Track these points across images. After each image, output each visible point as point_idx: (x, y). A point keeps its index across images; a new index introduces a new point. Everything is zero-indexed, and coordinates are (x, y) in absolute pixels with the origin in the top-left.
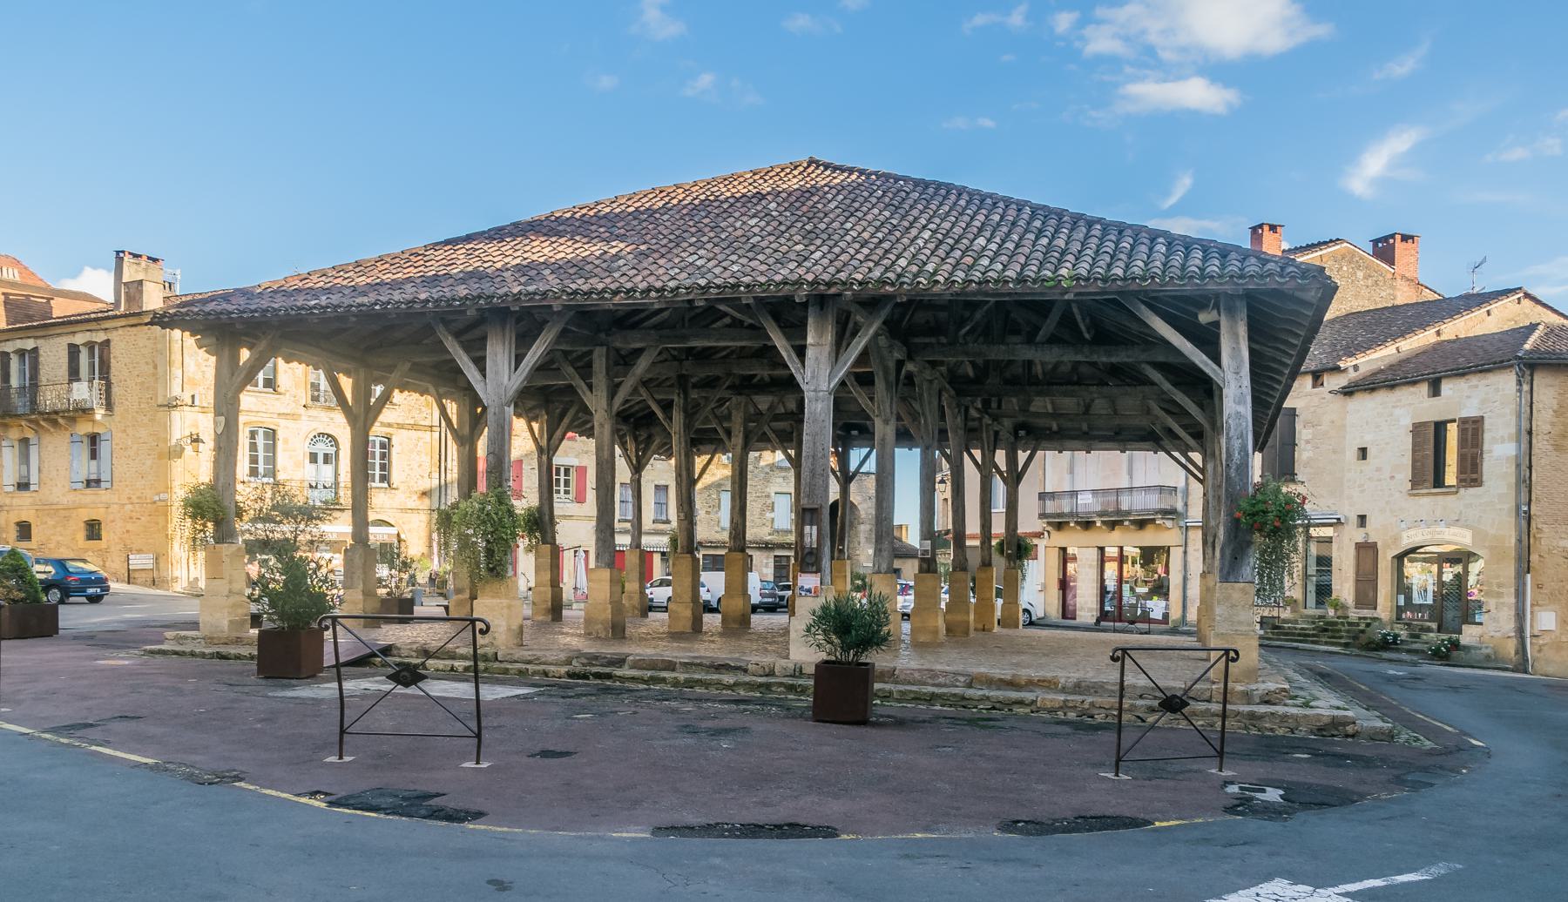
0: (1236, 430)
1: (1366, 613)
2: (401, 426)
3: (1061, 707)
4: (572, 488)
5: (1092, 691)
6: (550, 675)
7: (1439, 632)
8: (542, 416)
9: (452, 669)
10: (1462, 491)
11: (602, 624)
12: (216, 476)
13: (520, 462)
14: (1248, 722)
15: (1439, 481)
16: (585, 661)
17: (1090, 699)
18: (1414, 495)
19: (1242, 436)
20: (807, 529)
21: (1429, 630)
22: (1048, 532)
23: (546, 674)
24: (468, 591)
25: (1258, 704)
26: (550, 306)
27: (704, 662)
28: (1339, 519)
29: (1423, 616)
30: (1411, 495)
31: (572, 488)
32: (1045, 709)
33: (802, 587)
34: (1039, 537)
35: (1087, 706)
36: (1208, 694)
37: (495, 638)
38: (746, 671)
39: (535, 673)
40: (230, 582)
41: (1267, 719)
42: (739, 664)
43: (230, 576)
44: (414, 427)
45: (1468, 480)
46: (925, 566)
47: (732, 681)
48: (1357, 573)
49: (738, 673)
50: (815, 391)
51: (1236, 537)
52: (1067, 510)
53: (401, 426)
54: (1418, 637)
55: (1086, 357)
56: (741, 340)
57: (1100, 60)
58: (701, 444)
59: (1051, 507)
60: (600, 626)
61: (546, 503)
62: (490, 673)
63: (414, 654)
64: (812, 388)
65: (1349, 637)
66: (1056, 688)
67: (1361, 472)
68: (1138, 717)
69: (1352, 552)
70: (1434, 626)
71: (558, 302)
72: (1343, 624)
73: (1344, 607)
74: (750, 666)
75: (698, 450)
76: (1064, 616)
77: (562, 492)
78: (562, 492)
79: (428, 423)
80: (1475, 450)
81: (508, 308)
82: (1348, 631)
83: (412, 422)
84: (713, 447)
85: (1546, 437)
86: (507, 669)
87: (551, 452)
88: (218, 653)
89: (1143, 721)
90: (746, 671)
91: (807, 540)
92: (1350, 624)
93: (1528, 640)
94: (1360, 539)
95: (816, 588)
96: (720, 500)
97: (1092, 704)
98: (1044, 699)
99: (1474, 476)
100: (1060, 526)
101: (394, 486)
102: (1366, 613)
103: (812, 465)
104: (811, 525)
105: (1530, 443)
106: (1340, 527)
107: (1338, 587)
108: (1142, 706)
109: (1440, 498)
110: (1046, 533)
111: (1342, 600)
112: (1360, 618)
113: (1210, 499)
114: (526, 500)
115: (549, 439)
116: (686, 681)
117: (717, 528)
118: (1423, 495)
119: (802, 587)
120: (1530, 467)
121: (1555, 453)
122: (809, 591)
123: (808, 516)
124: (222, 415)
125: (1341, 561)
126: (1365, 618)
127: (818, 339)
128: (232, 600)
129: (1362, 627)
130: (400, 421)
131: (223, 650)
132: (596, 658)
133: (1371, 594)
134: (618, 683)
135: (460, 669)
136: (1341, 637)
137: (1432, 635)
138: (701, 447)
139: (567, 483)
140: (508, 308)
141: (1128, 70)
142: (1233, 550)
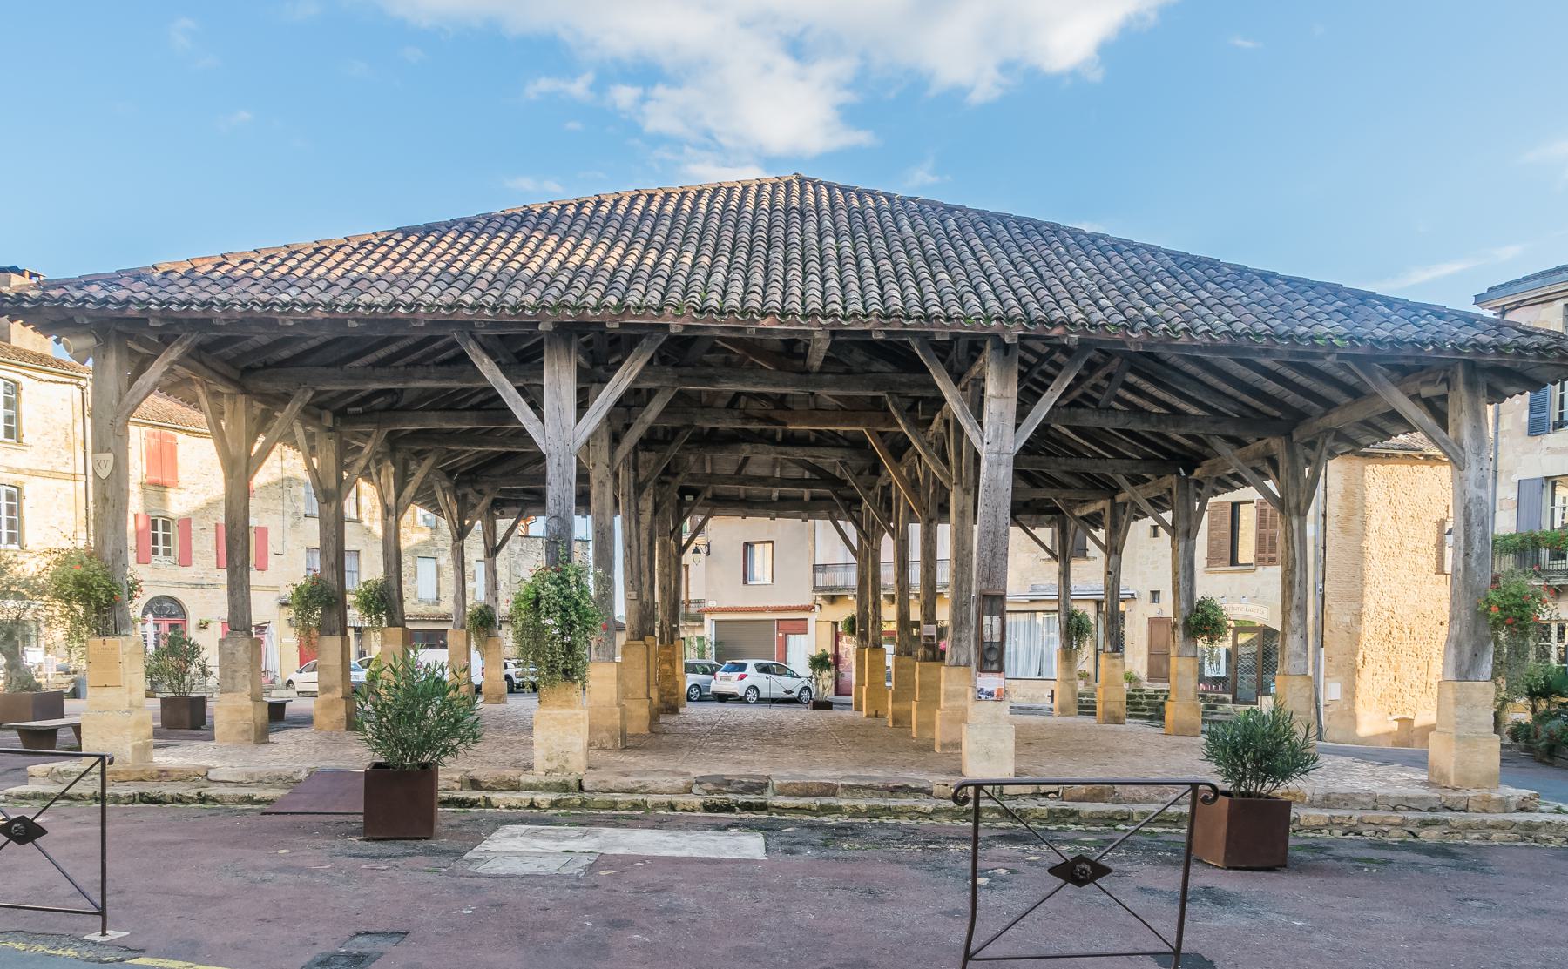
0: (1476, 516)
1: (1159, 685)
2: (34, 473)
3: (1326, 825)
4: (175, 547)
5: (1342, 803)
6: (677, 809)
7: (1233, 703)
8: (387, 467)
9: (532, 805)
10: (1260, 569)
11: (607, 730)
12: (101, 540)
13: (185, 523)
14: (1524, 833)
15: (1234, 561)
16: (710, 787)
17: (1357, 815)
18: (1211, 572)
19: (1483, 522)
20: (987, 619)
21: (1224, 701)
22: (820, 606)
23: (672, 807)
24: (340, 689)
25: (1514, 812)
26: (667, 326)
27: (876, 783)
28: (1132, 595)
29: (1217, 688)
30: (1206, 572)
31: (175, 547)
32: (1308, 828)
33: (982, 689)
34: (810, 611)
35: (1354, 823)
36: (1464, 803)
37: (567, 761)
38: (929, 793)
39: (656, 806)
40: (130, 692)
41: (1543, 829)
42: (921, 786)
43: (130, 681)
44: (52, 474)
45: (1267, 559)
46: (930, 653)
47: (930, 808)
48: (1150, 647)
49: (921, 796)
50: (998, 453)
51: (1475, 632)
52: (840, 583)
53: (34, 473)
54: (1214, 708)
55: (1154, 426)
56: (786, 386)
57: (659, 140)
58: (504, 506)
59: (823, 579)
60: (605, 734)
61: (394, 575)
62: (588, 808)
63: (457, 786)
64: (995, 449)
65: (1152, 710)
66: (1303, 802)
67: (1154, 548)
68: (1410, 832)
69: (1145, 626)
70: (1229, 697)
71: (679, 321)
72: (1141, 697)
73: (1137, 680)
74: (935, 788)
75: (502, 513)
76: (837, 693)
77: (161, 552)
78: (161, 552)
79: (69, 469)
80: (1274, 531)
81: (604, 324)
82: (1149, 704)
83: (49, 468)
84: (519, 509)
85: (1335, 520)
86: (615, 803)
87: (400, 513)
88: (141, 795)
89: (1415, 836)
90: (929, 793)
91: (986, 632)
92: (1148, 697)
93: (1322, 710)
94: (1153, 615)
95: (999, 690)
96: (416, 567)
97: (1361, 820)
98: (1307, 816)
99: (1272, 555)
100: (832, 600)
101: (28, 548)
102: (1159, 685)
103: (993, 542)
104: (991, 614)
105: (1325, 524)
106: (1133, 602)
107: (1131, 661)
108: (1414, 820)
109: (1237, 575)
110: (817, 608)
111: (1135, 674)
112: (1156, 691)
113: (1181, 580)
114: (367, 569)
115: (398, 496)
116: (869, 809)
117: (414, 600)
118: (1220, 572)
119: (982, 689)
120: (1324, 548)
121: (1342, 535)
122: (991, 694)
123: (988, 603)
124: (108, 450)
125: (1134, 636)
126: (1161, 691)
127: (1000, 392)
128: (135, 716)
129: (1161, 699)
130: (33, 467)
131: (151, 789)
132: (728, 783)
133: (1165, 667)
134: (775, 815)
135: (545, 805)
136: (1144, 710)
137: (1228, 706)
138: (504, 509)
139: (167, 540)
140: (604, 324)
141: (688, 149)
142: (1473, 647)
